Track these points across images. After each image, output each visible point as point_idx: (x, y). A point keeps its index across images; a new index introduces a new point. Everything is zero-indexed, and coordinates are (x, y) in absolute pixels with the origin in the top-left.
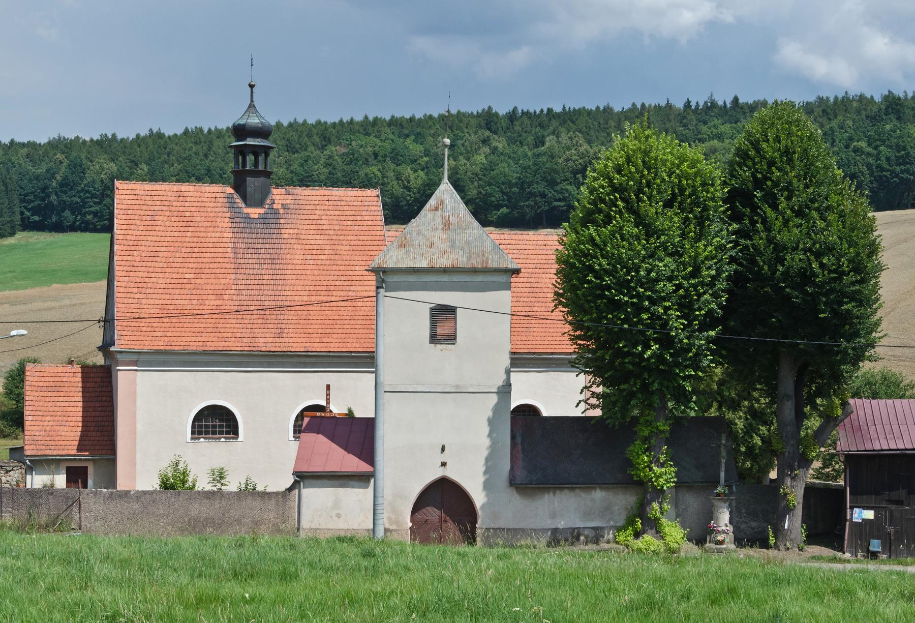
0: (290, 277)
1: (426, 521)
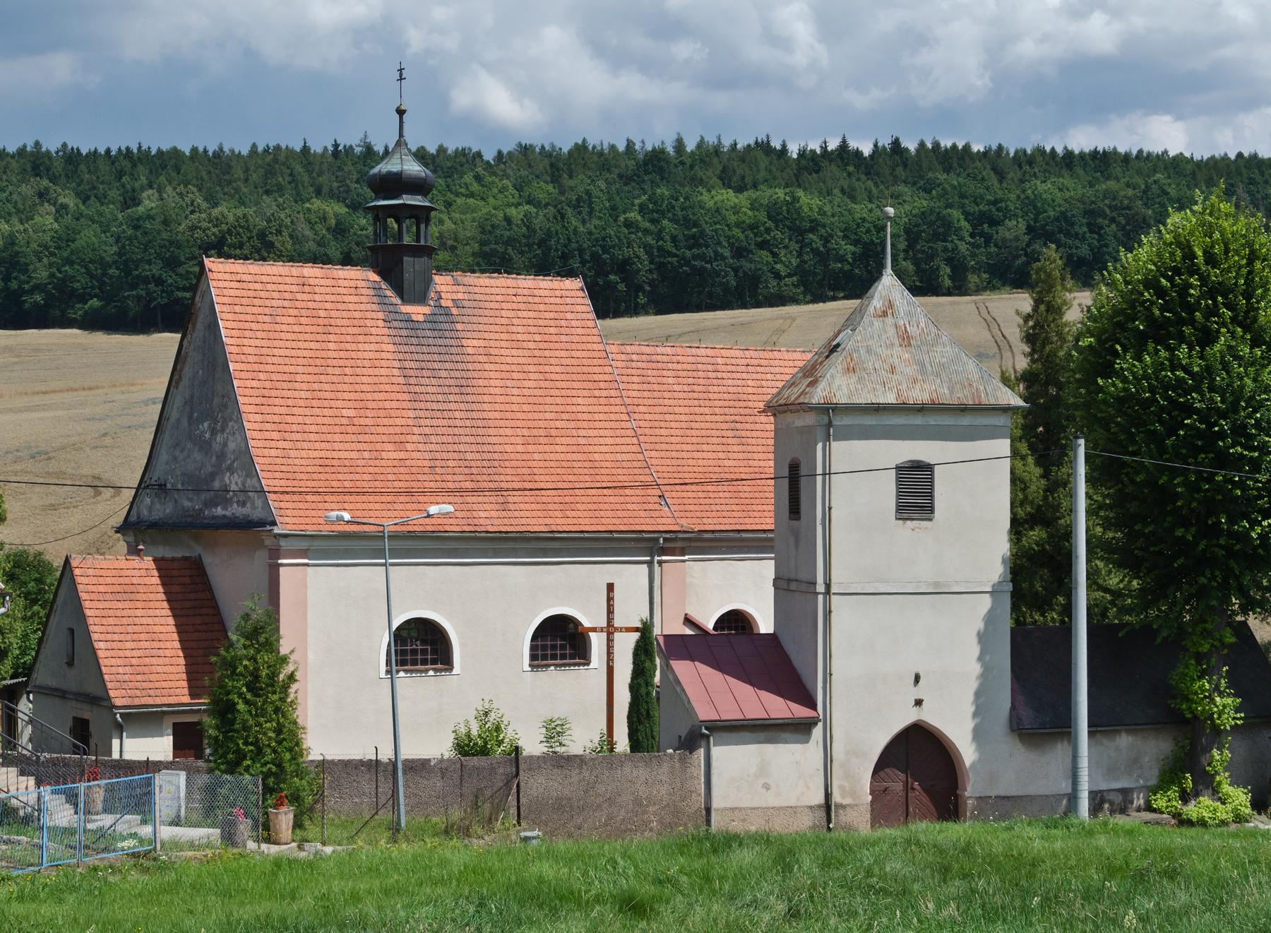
0: (491, 415)
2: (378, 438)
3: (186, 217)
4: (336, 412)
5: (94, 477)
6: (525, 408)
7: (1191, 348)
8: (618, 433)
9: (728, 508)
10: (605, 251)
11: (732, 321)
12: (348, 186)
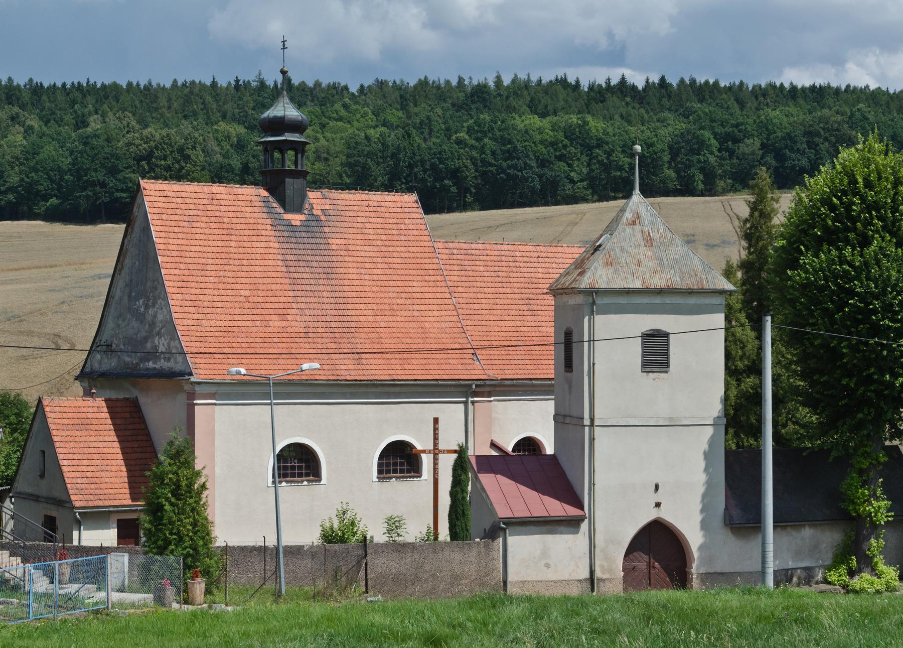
0: (349, 294)
1: (634, 568)
2: (267, 312)
3: (124, 136)
4: (236, 293)
5: (55, 335)
6: (375, 289)
7: (854, 249)
8: (443, 307)
9: (523, 362)
10: (441, 162)
11: (538, 215)
12: (247, 112)
